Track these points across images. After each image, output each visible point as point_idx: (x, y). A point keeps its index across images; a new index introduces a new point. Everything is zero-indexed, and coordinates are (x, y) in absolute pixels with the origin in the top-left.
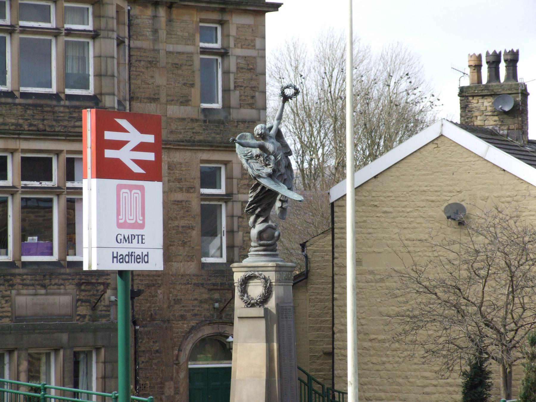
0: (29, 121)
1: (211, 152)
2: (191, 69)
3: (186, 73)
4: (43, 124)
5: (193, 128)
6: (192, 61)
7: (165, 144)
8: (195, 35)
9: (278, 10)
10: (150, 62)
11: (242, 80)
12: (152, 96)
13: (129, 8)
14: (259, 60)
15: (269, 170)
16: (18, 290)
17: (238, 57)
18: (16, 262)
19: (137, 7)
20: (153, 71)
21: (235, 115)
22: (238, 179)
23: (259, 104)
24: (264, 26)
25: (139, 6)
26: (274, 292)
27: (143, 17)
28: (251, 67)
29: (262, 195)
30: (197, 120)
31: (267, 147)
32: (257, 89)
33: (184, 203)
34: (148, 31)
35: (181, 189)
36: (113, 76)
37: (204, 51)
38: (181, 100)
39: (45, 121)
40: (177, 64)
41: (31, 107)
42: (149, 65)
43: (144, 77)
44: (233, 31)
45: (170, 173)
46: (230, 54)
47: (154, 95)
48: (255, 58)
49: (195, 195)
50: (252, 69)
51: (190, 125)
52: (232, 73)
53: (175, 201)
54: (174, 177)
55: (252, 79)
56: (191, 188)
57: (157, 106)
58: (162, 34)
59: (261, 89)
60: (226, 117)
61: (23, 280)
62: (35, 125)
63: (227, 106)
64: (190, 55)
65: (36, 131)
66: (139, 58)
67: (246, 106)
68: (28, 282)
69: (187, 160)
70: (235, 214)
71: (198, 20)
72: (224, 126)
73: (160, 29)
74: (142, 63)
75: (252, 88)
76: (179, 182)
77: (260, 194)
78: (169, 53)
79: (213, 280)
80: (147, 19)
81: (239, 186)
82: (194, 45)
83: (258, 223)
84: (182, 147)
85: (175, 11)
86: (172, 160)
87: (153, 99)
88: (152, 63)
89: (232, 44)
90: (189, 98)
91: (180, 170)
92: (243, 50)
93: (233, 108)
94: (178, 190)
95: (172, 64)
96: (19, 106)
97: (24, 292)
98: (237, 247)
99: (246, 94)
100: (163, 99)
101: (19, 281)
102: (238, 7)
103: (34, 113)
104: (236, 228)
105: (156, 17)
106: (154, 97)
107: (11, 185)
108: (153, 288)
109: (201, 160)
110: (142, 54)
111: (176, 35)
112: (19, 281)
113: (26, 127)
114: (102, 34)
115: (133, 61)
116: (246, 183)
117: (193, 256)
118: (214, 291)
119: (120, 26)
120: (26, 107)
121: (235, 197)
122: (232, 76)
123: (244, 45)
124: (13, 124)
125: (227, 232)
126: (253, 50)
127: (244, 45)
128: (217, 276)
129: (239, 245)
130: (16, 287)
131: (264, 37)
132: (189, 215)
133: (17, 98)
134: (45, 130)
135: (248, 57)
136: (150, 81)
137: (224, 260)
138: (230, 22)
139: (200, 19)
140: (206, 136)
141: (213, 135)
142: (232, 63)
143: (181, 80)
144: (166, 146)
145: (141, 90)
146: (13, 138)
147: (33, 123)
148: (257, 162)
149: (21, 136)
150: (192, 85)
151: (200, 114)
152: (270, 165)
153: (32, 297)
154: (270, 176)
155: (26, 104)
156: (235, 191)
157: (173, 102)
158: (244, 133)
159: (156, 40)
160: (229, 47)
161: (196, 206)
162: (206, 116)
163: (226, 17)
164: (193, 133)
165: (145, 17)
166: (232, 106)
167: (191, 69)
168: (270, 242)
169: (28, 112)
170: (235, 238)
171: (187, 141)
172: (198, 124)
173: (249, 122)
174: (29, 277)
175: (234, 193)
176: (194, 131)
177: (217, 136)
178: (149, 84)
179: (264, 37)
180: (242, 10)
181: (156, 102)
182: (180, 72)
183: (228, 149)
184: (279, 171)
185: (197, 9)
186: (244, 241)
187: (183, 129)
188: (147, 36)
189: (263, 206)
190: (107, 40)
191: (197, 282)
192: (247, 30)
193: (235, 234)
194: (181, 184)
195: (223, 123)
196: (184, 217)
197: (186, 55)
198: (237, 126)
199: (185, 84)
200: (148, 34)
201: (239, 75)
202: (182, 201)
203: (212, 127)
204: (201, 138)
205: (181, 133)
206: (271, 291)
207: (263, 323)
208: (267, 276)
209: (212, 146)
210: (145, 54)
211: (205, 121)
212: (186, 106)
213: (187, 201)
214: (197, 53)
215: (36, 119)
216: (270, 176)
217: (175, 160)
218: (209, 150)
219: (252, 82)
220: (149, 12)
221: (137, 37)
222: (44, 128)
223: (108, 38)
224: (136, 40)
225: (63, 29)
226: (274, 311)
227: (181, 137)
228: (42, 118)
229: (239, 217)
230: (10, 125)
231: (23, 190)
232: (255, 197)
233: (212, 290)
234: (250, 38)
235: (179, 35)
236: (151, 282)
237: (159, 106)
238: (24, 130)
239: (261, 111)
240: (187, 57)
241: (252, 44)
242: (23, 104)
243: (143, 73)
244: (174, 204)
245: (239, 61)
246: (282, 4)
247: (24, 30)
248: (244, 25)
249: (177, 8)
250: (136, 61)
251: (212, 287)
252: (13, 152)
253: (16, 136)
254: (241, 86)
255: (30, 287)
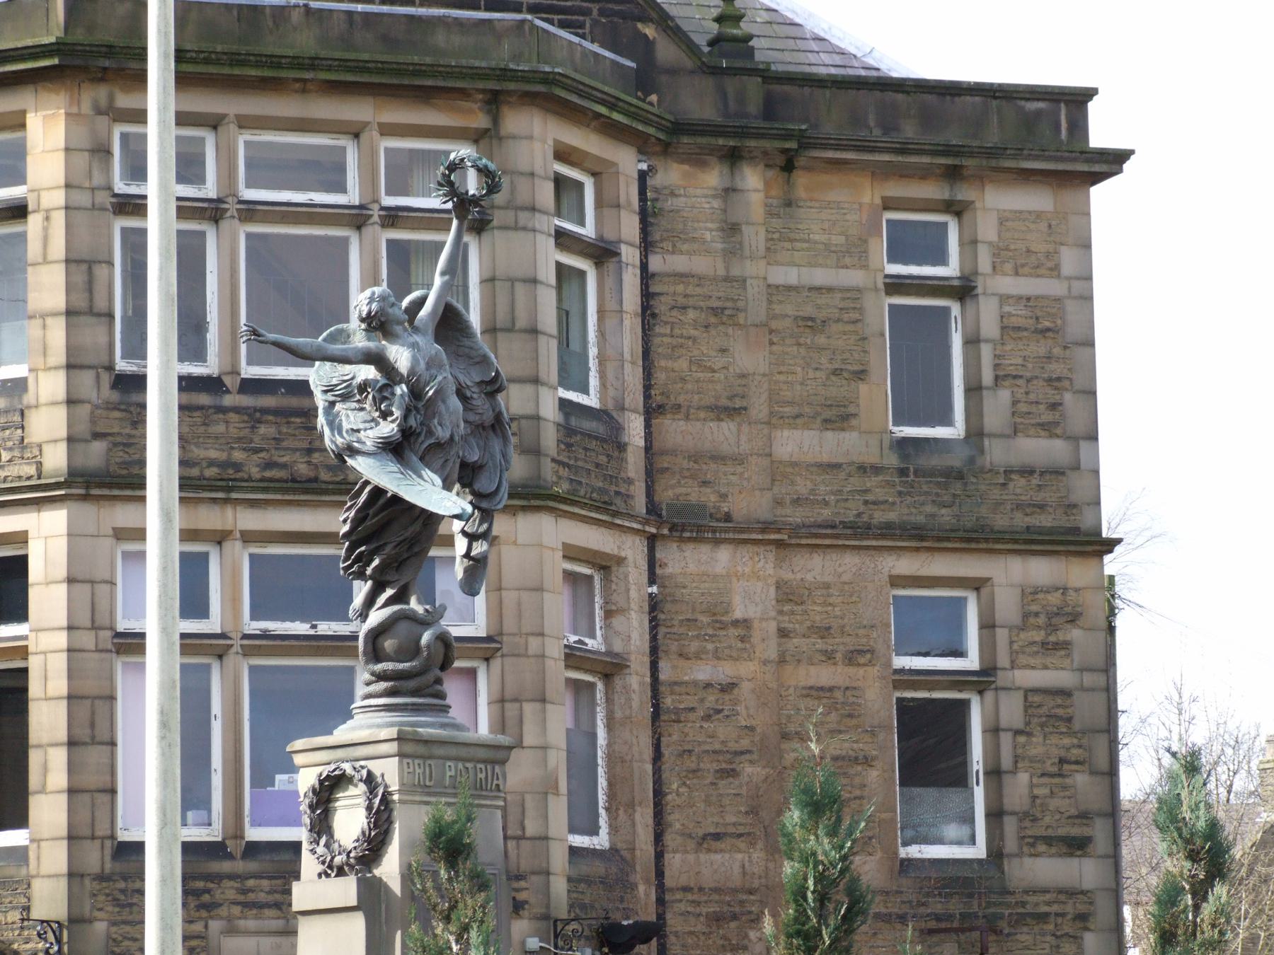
0: (263, 455)
1: (923, 556)
2: (856, 332)
3: (840, 342)
4: (309, 463)
5: (866, 491)
6: (861, 310)
7: (763, 531)
8: (866, 241)
9: (1036, 141)
10: (715, 311)
11: (1020, 361)
12: (724, 402)
13: (644, 166)
14: (1071, 306)
15: (388, 428)
16: (229, 919)
17: (1004, 299)
18: (228, 842)
19: (675, 165)
20: (727, 334)
21: (997, 453)
22: (1011, 628)
23: (1076, 424)
24: (1088, 214)
25: (682, 162)
26: (397, 825)
27: (691, 191)
28: (1047, 324)
29: (376, 515)
30: (877, 470)
31: (392, 359)
32: (1066, 383)
33: (838, 694)
34: (706, 229)
35: (829, 656)
36: (534, 331)
37: (896, 286)
38: (828, 414)
39: (316, 455)
40: (812, 319)
41: (271, 418)
42: (713, 320)
43: (696, 352)
44: (987, 229)
45: (781, 612)
46: (979, 290)
47: (731, 398)
48: (1058, 300)
49: (874, 671)
50: (1048, 330)
51: (856, 482)
52: (987, 341)
53: (811, 688)
54: (808, 623)
55: (1049, 358)
56: (861, 652)
57: (739, 431)
58: (755, 237)
59: (1079, 383)
60: (972, 460)
61: (245, 892)
62: (284, 466)
63: (975, 433)
64: (854, 295)
65: (286, 481)
66: (681, 300)
67: (1032, 431)
68: (262, 897)
69: (845, 578)
70: (1004, 723)
71: (878, 201)
72: (966, 484)
73: (748, 223)
74: (691, 314)
75: (1049, 380)
76: (822, 638)
77: (371, 512)
78: (774, 290)
79: (937, 906)
80: (706, 196)
81: (1015, 647)
82: (865, 267)
83: (377, 606)
84: (827, 542)
85: (801, 180)
86: (799, 576)
87: (726, 409)
88: (722, 315)
89: (984, 264)
90: (852, 409)
91: (825, 604)
92: (1022, 280)
93: (991, 435)
94: (820, 657)
95: (796, 318)
96: (232, 415)
97: (251, 924)
98: (1013, 813)
99: (1032, 397)
100: (759, 407)
101: (231, 894)
102: (993, 163)
103: (280, 433)
104: (1006, 762)
105: (734, 190)
106: (730, 404)
107: (219, 631)
108: (733, 925)
109: (890, 576)
110: (690, 290)
111: (808, 241)
112: (231, 894)
113: (255, 472)
114: (498, 217)
115: (661, 306)
116: (1038, 639)
117: (870, 838)
118: (942, 936)
119: (606, 211)
120: (254, 417)
121: (1002, 678)
122: (986, 352)
123: (1023, 266)
124: (212, 463)
125: (986, 773)
126: (1055, 281)
127: (1023, 266)
128: (951, 895)
129: (1017, 809)
130: (223, 911)
131: (1085, 245)
132: (858, 726)
133: (228, 391)
134: (316, 480)
135: (1037, 298)
136: (719, 362)
137: (979, 851)
138: (978, 205)
139: (884, 199)
140: (906, 511)
141: (929, 509)
142: (988, 315)
143: (823, 360)
144: (767, 537)
145: (689, 386)
146: (214, 500)
147: (276, 459)
148: (362, 409)
149: (234, 495)
150: (861, 375)
151: (886, 451)
152: (392, 414)
153: (278, 940)
154: (395, 449)
155: (255, 410)
156: (1003, 659)
157: (799, 421)
158: (340, 326)
159: (733, 251)
160: (976, 273)
161: (880, 704)
162: (904, 457)
163: (964, 193)
164: (866, 502)
165: (699, 192)
166: (986, 430)
167: (856, 332)
168: (401, 666)
169: (263, 430)
170: (1007, 791)
171: (845, 525)
172: (881, 478)
173: (1042, 474)
174: (265, 883)
175: (999, 665)
176: (870, 497)
177: (944, 511)
178: (714, 371)
179: (1087, 246)
180: (1009, 170)
181: (738, 419)
182: (821, 340)
183: (973, 546)
184: (430, 433)
185: (873, 174)
186: (1035, 797)
187: (832, 493)
188: (705, 242)
189: (388, 549)
190: (511, 234)
191: (883, 910)
192: (1032, 226)
193: (1007, 779)
194: (830, 641)
195: (960, 476)
196: (840, 732)
197: (839, 295)
198: (1004, 484)
199: (837, 372)
200: (708, 236)
201: (1008, 348)
202: (831, 689)
203: (925, 488)
204: (892, 516)
205: (826, 503)
206: (390, 822)
207: (357, 925)
208: (377, 773)
209: (922, 538)
210: (698, 290)
211: (903, 472)
212: (843, 430)
213: (847, 688)
214: (876, 289)
215: (288, 449)
216: (395, 449)
217: (809, 577)
218: (917, 549)
219: (1053, 366)
220: (713, 177)
221: (674, 246)
222: (312, 474)
223: (516, 228)
224: (673, 253)
225: (376, 207)
226: (396, 886)
227: (826, 514)
228: (305, 445)
229: (1017, 732)
230: (204, 464)
231: (246, 642)
232: (357, 522)
233: (931, 932)
234: (1040, 247)
235: (816, 242)
236: (726, 908)
237: (745, 428)
238: (250, 479)
239: (1084, 445)
240: (843, 299)
241: (1050, 264)
242: (249, 408)
243: (694, 339)
244: (808, 696)
245: (1007, 309)
246: (1132, 152)
247: (251, 211)
248: (1021, 212)
249: (808, 169)
250: (673, 308)
251: (933, 924)
252: (220, 538)
253: (220, 495)
254: (1015, 377)
255: (267, 912)
